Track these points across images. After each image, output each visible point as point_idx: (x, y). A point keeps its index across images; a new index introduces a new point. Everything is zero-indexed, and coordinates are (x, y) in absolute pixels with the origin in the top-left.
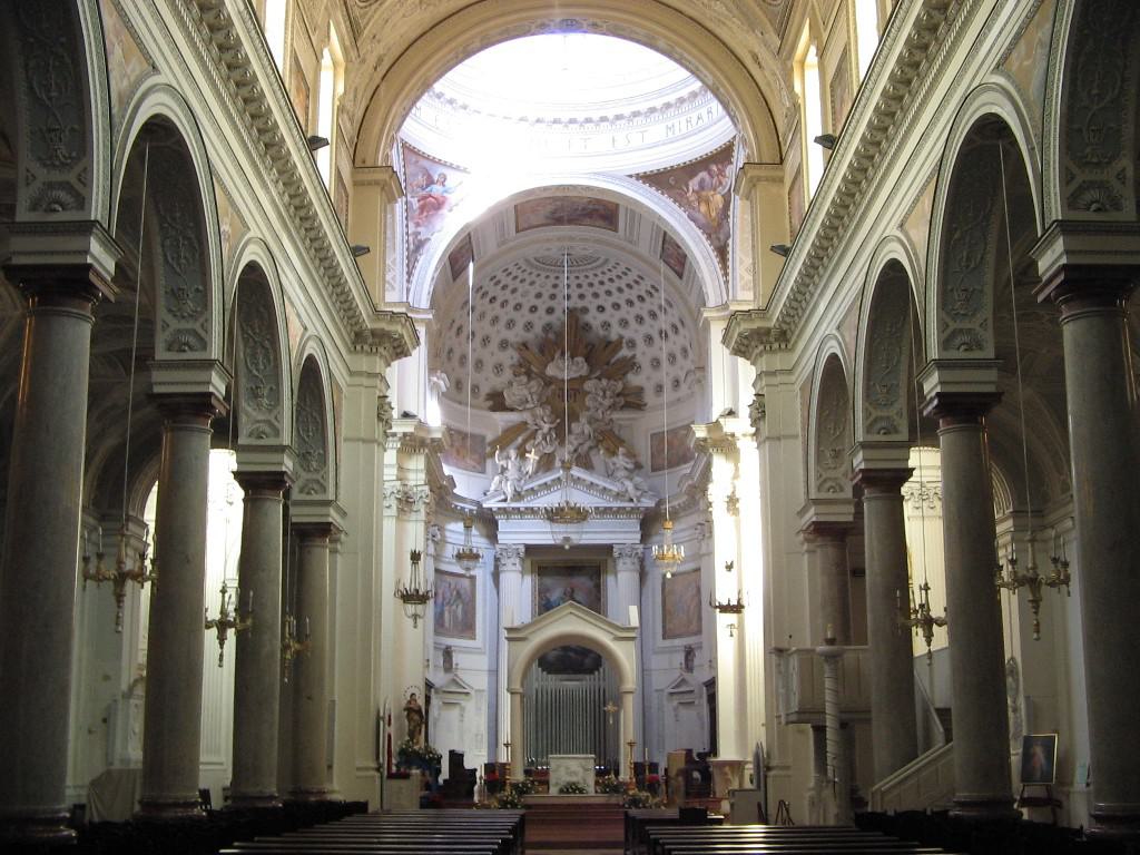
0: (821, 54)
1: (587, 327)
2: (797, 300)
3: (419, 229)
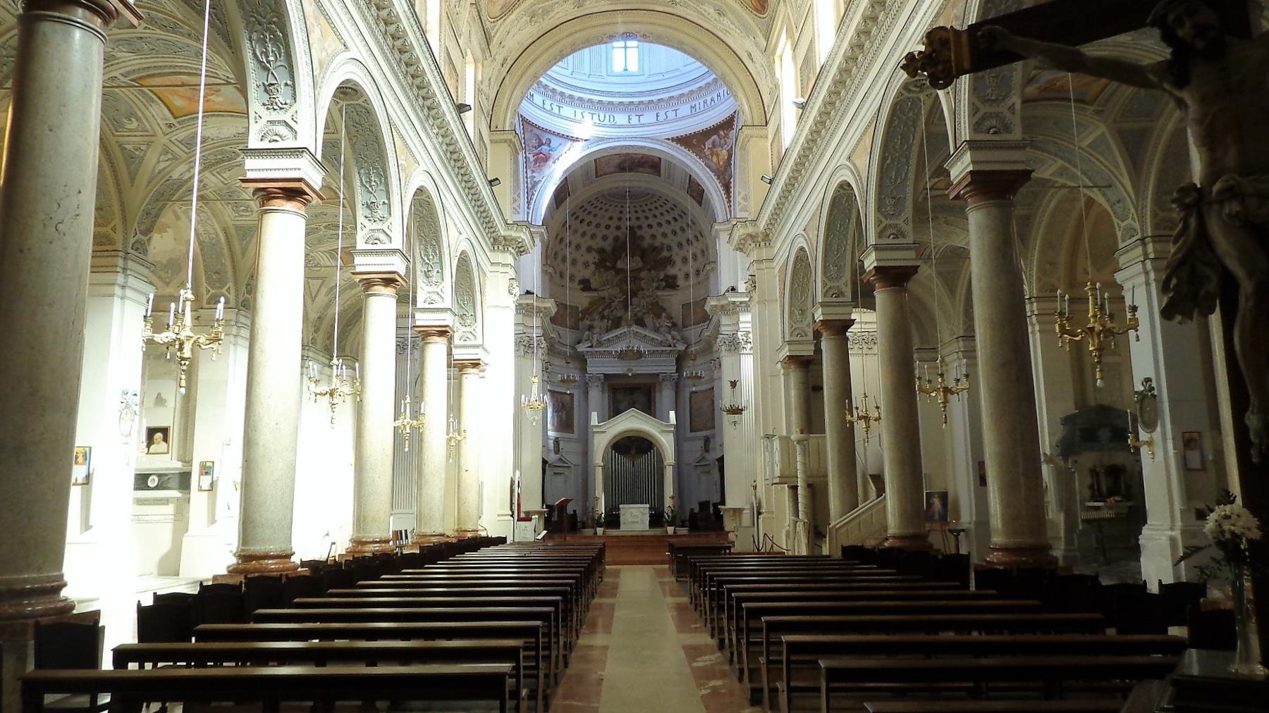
0: (795, 48)
1: (642, 238)
2: (776, 214)
3: (534, 174)
